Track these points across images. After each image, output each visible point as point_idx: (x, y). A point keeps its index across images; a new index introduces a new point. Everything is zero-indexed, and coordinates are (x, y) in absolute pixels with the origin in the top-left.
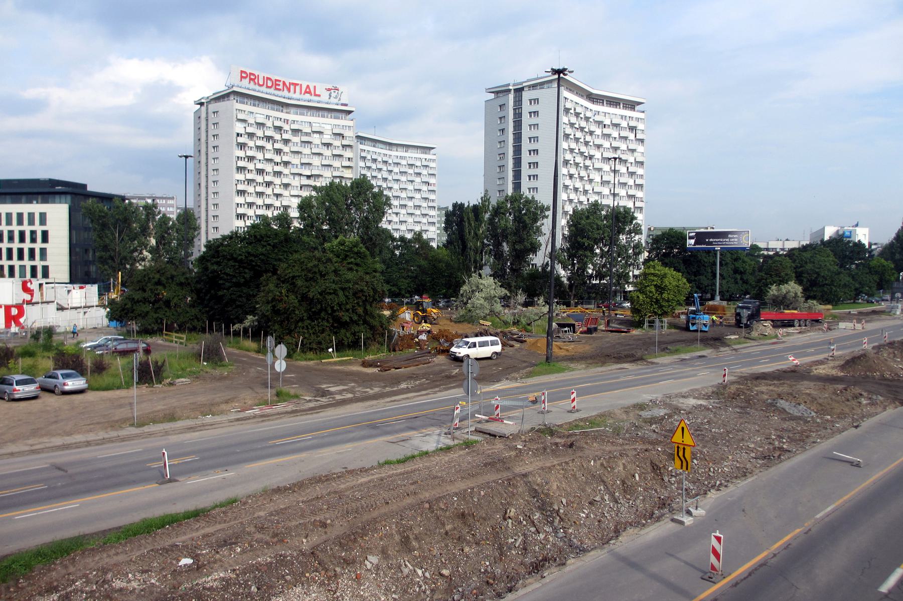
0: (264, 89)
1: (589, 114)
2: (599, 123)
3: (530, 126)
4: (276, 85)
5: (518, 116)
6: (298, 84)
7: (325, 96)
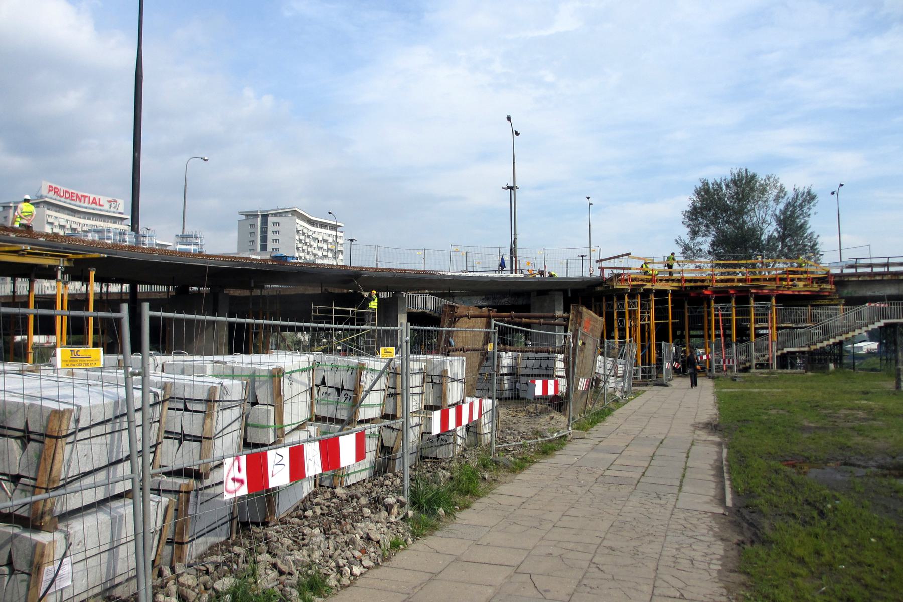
0: (63, 199)
1: (310, 234)
2: (315, 239)
3: (273, 240)
4: (72, 196)
5: (264, 232)
6: (87, 196)
7: (107, 206)
